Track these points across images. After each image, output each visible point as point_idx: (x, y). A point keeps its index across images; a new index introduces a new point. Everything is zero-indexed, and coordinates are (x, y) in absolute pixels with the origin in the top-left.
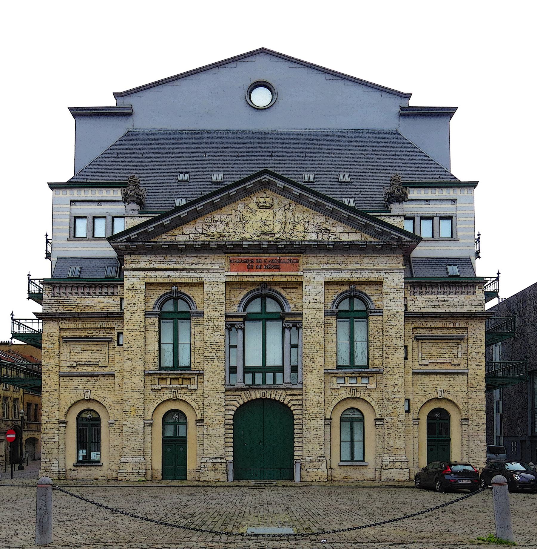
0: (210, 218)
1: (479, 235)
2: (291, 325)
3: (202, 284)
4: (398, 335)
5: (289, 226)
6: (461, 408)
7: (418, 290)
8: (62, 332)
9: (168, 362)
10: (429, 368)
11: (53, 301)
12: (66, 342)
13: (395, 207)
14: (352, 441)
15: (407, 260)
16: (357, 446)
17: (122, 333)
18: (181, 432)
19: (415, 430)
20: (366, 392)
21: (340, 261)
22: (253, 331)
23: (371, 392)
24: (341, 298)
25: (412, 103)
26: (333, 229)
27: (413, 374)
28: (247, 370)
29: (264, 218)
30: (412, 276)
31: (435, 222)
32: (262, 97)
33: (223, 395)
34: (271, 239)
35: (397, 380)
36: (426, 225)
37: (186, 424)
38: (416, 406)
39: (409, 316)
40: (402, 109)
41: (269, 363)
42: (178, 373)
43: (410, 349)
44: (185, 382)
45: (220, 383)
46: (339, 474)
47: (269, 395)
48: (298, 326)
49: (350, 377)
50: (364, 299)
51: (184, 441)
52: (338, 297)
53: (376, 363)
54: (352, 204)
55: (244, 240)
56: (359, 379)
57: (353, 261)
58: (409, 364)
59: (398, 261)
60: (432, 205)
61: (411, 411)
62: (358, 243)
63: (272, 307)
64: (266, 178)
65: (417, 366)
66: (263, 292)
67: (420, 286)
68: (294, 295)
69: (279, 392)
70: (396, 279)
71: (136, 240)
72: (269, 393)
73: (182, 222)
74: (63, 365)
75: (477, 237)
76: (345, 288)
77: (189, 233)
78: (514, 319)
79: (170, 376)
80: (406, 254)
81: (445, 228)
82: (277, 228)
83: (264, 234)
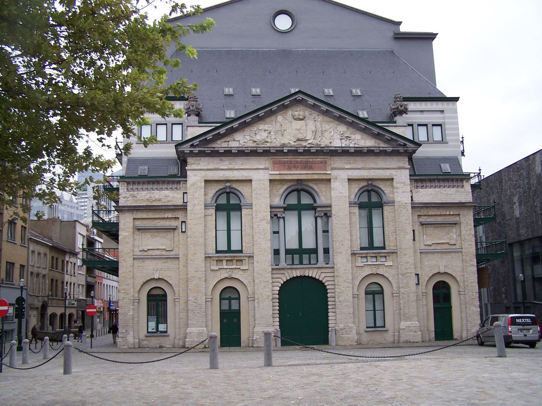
0: (254, 128)
1: (463, 138)
2: (322, 214)
3: (251, 181)
4: (408, 222)
5: (319, 134)
6: (458, 280)
7: (420, 184)
8: (135, 221)
9: (223, 246)
10: (432, 248)
11: (128, 195)
12: (138, 229)
13: (399, 119)
14: (374, 310)
15: (410, 160)
16: (379, 314)
17: (185, 222)
18: (234, 307)
19: (424, 300)
20: (385, 269)
21: (359, 162)
22: (291, 220)
23: (387, 267)
24: (362, 191)
25: (403, 29)
26: (353, 137)
27: (421, 253)
28: (288, 252)
29: (298, 128)
30: (415, 173)
31: (429, 128)
32: (283, 23)
33: (270, 273)
34: (304, 144)
35: (408, 258)
36: (422, 131)
37: (239, 299)
38: (424, 279)
39: (415, 206)
40: (395, 34)
41: (304, 246)
42: (230, 254)
43: (416, 232)
44: (239, 263)
45: (267, 264)
46: (365, 338)
47: (307, 273)
48: (327, 216)
49: (371, 257)
50: (378, 193)
51: (237, 313)
52: (359, 191)
53: (390, 246)
54: (366, 116)
55: (283, 145)
56: (378, 258)
57: (371, 162)
58: (417, 245)
59: (404, 162)
60: (426, 115)
61: (420, 284)
62: (373, 149)
63: (306, 200)
64: (300, 97)
65: (423, 247)
66: (300, 187)
67: (421, 181)
68: (323, 189)
69: (316, 270)
70: (402, 176)
71: (197, 146)
72: (307, 271)
73: (232, 131)
74: (136, 249)
75: (461, 140)
76: (364, 184)
77: (241, 140)
78: (494, 206)
79: (226, 259)
80: (410, 155)
81: (437, 133)
82: (309, 136)
83: (299, 140)
